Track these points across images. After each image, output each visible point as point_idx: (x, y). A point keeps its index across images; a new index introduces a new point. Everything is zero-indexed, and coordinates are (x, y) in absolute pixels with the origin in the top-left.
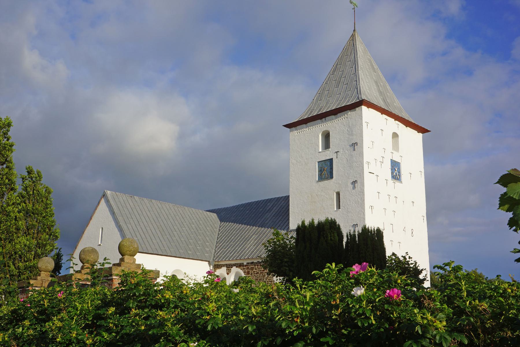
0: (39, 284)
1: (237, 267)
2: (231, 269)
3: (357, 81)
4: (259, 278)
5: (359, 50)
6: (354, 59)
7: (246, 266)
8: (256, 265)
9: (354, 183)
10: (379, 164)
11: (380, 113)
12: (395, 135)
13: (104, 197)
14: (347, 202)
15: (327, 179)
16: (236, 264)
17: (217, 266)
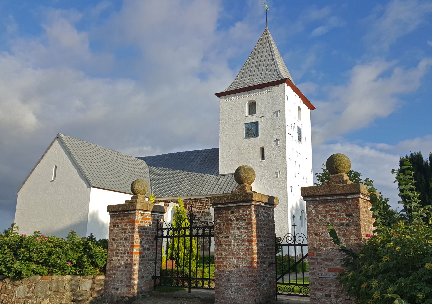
0: (145, 207)
1: (174, 202)
2: (168, 204)
3: (275, 65)
4: (196, 211)
6: (270, 49)
8: (193, 201)
9: (277, 141)
10: (293, 128)
13: (58, 138)
15: (252, 137)
16: (173, 200)
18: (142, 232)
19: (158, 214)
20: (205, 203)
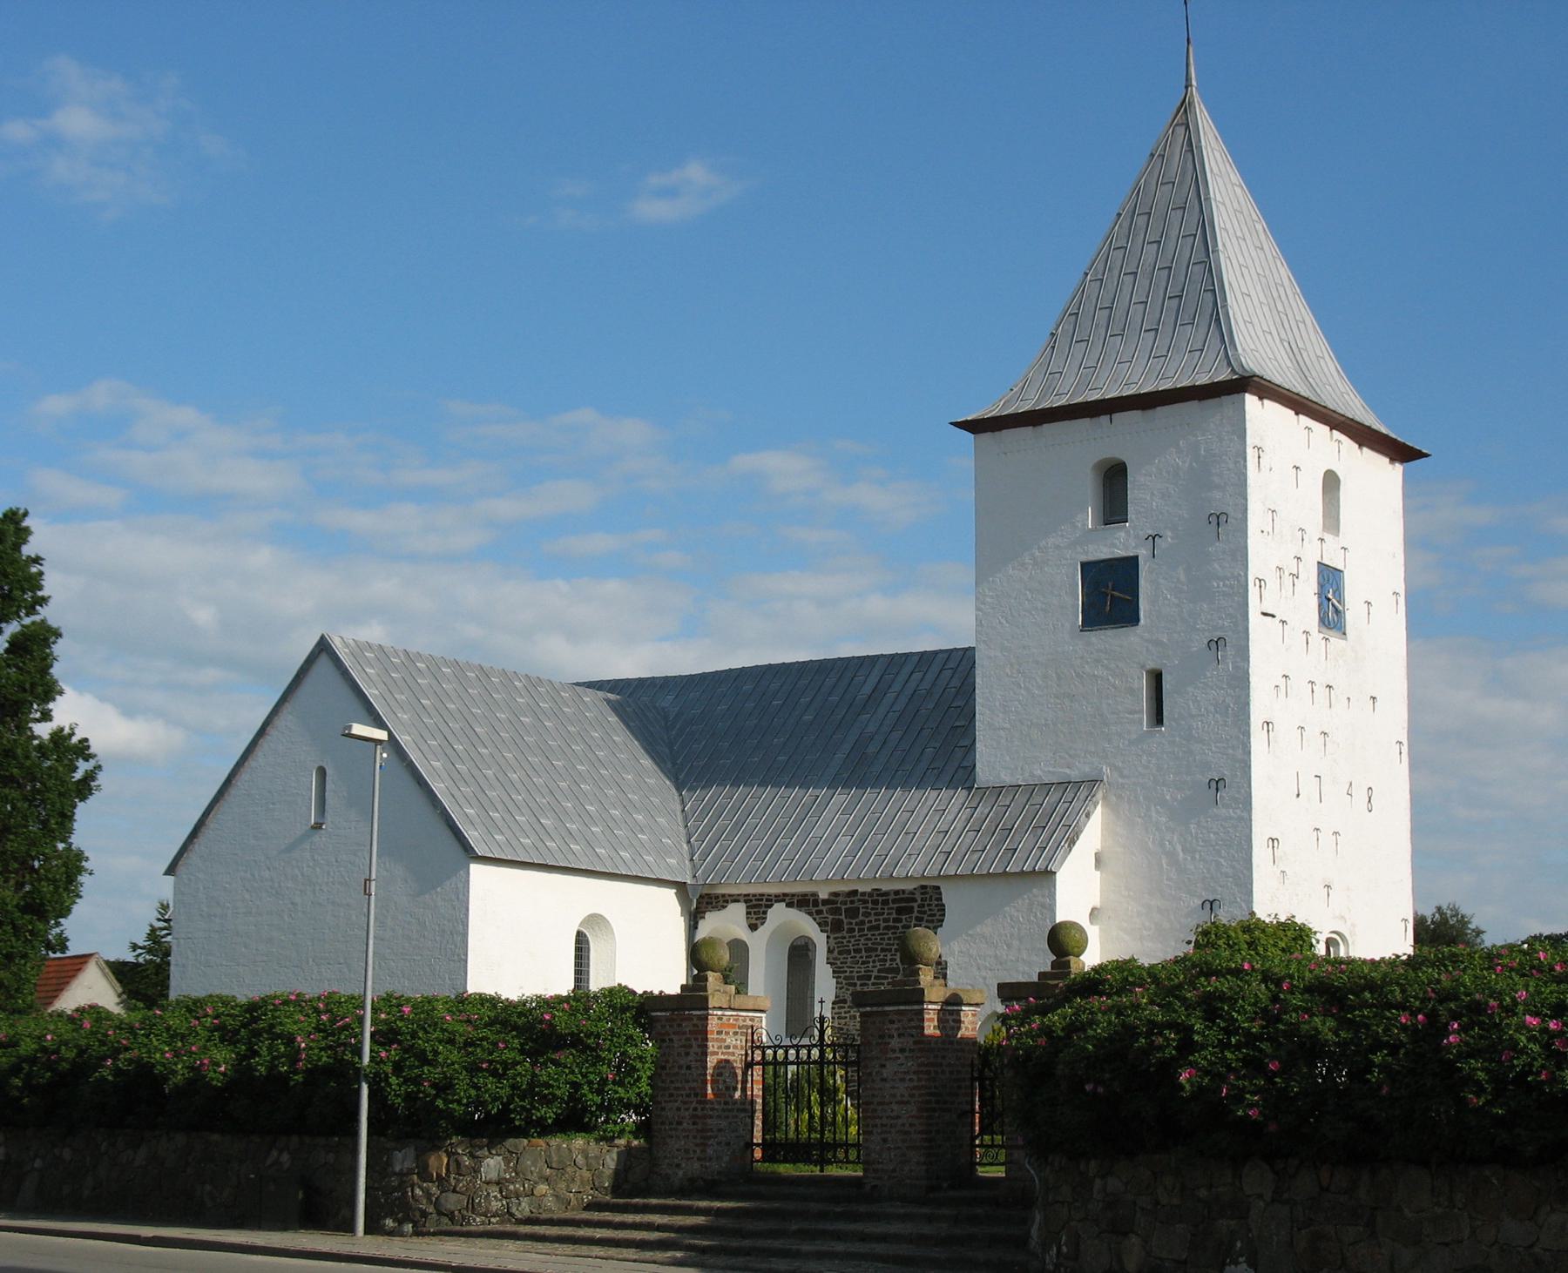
1: (789, 905)
2: (765, 913)
5: (1211, 170)
7: (825, 902)
9: (1216, 644)
10: (1288, 580)
11: (1293, 413)
12: (1331, 482)
14: (1189, 706)
16: (785, 895)
17: (706, 900)
18: (722, 1053)
19: (751, 1014)
20: (916, 909)
